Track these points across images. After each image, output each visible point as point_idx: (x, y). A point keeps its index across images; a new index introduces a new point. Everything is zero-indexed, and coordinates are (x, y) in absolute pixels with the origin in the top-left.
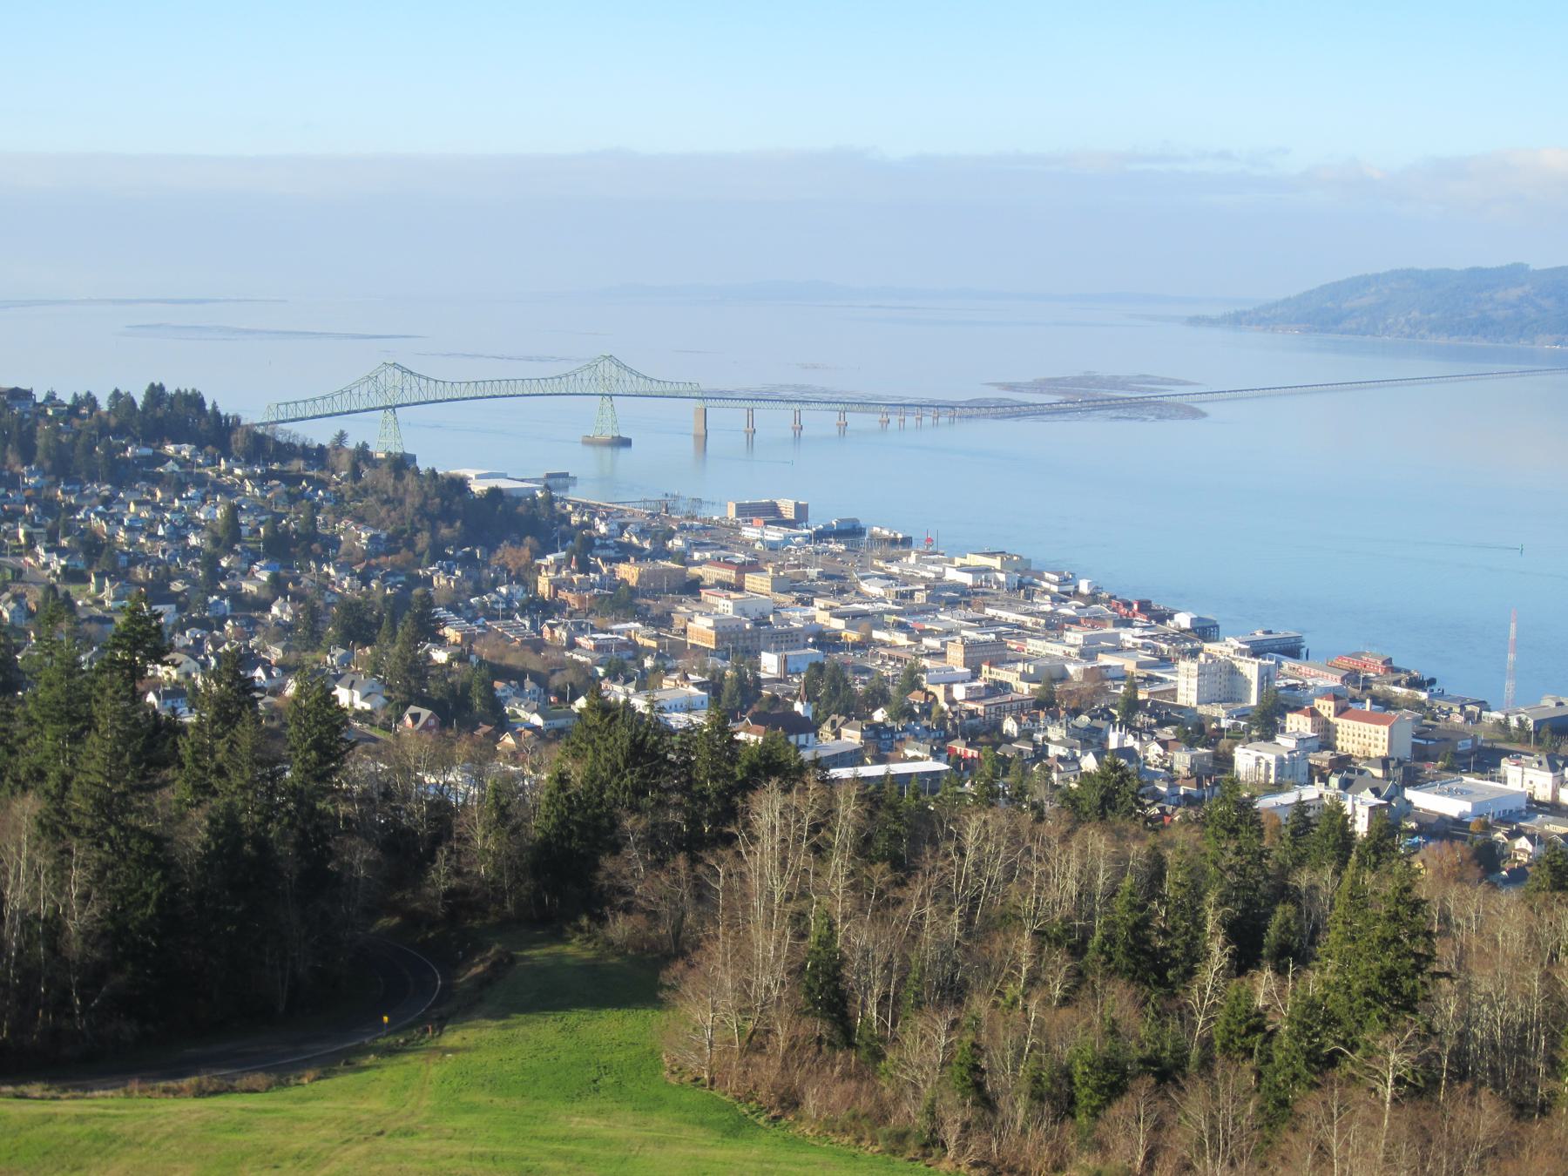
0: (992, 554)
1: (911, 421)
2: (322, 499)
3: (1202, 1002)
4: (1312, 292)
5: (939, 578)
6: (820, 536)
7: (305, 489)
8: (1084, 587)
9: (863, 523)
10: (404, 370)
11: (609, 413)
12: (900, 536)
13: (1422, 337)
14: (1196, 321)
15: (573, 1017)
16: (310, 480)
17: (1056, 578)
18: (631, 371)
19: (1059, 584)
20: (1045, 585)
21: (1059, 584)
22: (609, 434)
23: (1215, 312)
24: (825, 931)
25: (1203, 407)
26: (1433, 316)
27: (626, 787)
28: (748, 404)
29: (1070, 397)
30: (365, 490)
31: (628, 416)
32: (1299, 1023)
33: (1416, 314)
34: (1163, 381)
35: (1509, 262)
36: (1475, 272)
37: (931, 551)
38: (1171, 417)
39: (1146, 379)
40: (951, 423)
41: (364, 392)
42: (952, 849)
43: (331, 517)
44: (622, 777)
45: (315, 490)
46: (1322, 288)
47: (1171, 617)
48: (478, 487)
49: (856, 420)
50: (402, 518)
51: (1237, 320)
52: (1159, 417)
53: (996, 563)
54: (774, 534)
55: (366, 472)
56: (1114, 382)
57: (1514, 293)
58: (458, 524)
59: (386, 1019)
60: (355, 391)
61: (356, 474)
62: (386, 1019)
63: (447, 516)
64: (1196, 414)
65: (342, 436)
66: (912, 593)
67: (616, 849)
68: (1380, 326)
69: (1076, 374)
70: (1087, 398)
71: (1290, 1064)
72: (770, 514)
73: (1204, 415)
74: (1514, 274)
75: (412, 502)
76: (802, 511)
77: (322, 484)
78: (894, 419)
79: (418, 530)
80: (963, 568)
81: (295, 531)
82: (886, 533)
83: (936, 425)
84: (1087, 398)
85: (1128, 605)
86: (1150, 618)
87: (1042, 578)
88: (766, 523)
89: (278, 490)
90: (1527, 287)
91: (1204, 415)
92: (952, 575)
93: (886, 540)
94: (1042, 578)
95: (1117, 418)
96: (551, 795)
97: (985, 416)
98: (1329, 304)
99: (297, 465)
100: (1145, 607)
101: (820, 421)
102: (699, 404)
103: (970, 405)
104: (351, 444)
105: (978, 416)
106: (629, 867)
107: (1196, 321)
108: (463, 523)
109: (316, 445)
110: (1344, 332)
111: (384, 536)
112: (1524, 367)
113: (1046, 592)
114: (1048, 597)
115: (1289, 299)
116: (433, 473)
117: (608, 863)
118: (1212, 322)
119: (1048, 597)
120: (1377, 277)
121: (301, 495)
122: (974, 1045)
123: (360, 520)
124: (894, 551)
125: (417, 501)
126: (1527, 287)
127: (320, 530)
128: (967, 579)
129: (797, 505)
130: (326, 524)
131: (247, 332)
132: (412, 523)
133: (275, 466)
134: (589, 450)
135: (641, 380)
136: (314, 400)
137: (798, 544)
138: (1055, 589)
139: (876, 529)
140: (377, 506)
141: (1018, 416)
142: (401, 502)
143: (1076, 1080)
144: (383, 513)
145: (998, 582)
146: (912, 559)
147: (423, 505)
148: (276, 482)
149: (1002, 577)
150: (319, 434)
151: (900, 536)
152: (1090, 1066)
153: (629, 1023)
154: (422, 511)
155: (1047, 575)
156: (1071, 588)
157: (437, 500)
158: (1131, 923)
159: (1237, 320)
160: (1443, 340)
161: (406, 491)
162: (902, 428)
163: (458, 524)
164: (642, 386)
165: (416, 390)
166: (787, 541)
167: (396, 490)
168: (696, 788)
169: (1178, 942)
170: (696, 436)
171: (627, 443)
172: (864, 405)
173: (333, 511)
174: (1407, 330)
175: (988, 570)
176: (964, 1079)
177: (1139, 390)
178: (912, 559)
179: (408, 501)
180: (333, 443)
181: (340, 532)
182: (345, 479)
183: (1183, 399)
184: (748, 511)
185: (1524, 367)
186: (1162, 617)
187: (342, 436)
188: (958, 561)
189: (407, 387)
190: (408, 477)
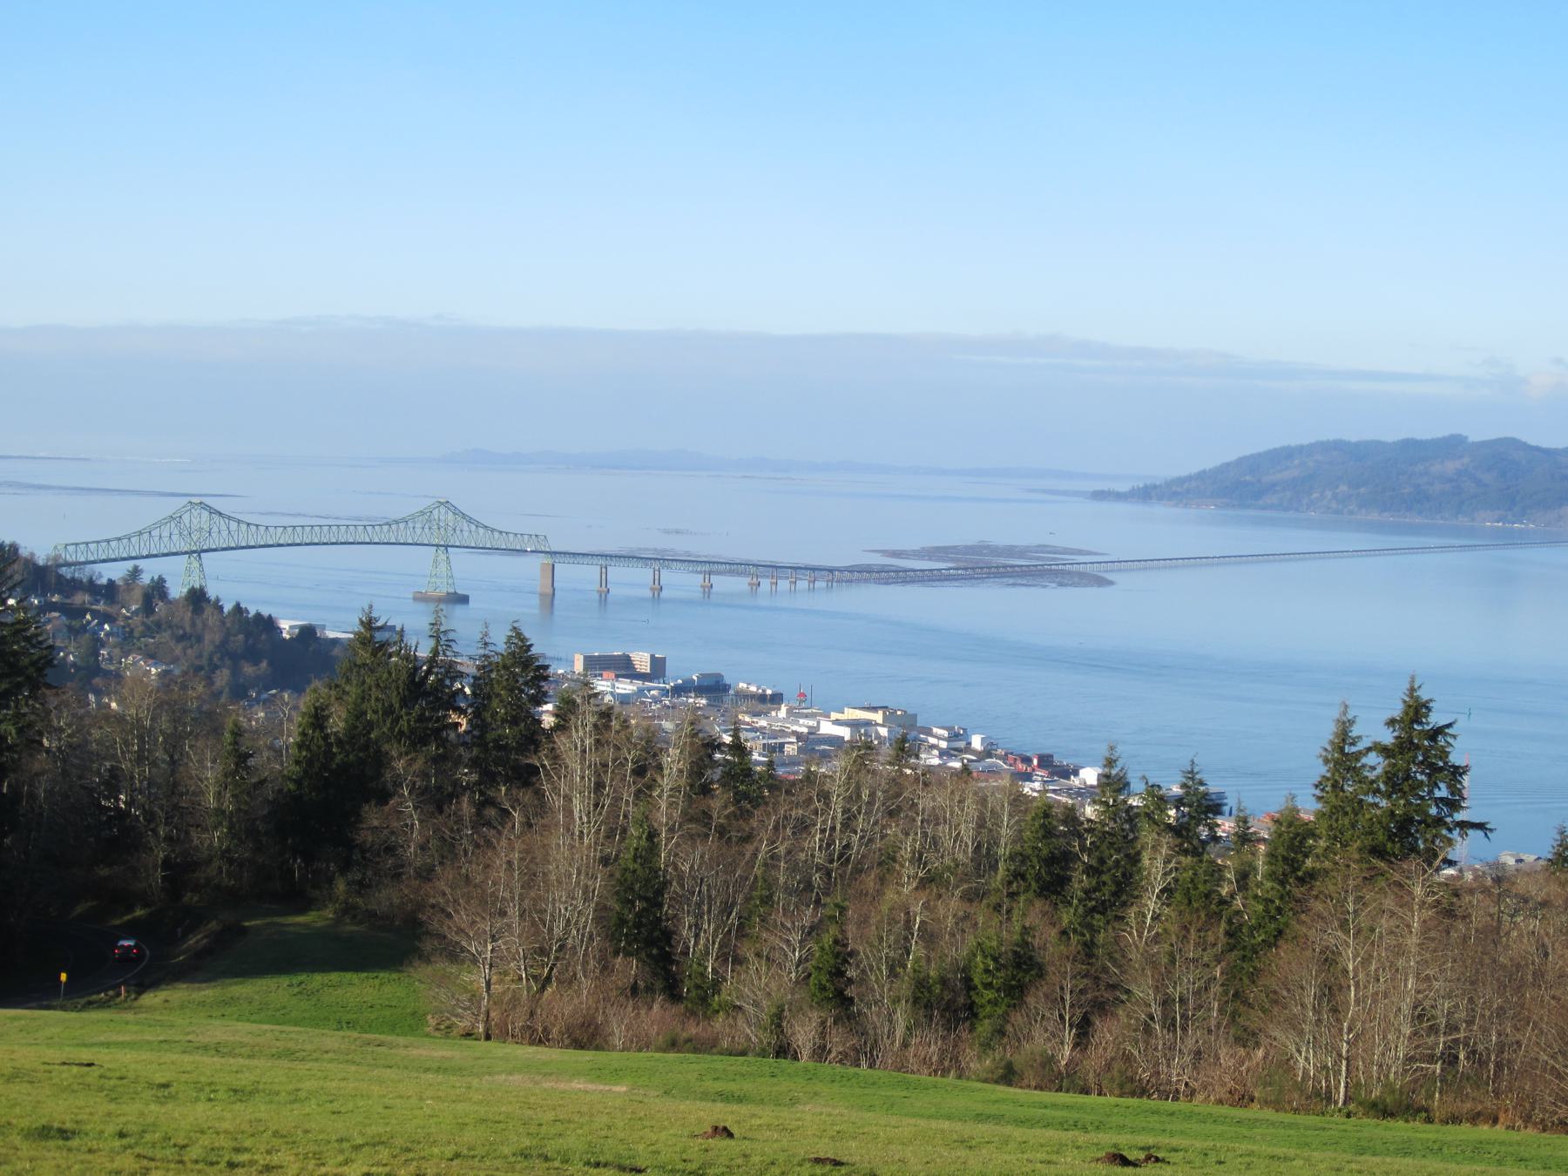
0: (874, 709)
1: (784, 585)
2: (108, 634)
3: (1140, 937)
4: (1228, 464)
5: (813, 731)
6: (678, 691)
7: (89, 622)
8: (977, 742)
9: (727, 681)
10: (213, 511)
11: (443, 567)
12: (769, 692)
13: (1351, 513)
14: (1100, 495)
15: (318, 979)
16: (95, 614)
17: (945, 733)
18: (470, 521)
19: (949, 740)
20: (932, 741)
21: (949, 740)
22: (443, 590)
23: (1123, 487)
24: (643, 843)
25: (1110, 577)
26: (1362, 490)
27: (401, 733)
28: (602, 562)
29: (962, 565)
30: (158, 625)
31: (467, 570)
32: (1285, 859)
33: (1343, 488)
34: (1066, 551)
35: (1446, 433)
36: (1408, 445)
37: (803, 703)
38: (1074, 585)
39: (1042, 548)
40: (829, 588)
41: (166, 534)
42: (814, 794)
43: (117, 651)
44: (397, 720)
45: (101, 624)
46: (1240, 461)
47: (1076, 773)
48: (287, 626)
49: (722, 583)
50: (200, 656)
51: (1147, 494)
52: (1061, 585)
53: (878, 717)
54: (626, 687)
55: (160, 607)
56: (1010, 551)
57: (1451, 466)
58: (264, 664)
59: (64, 977)
60: (155, 533)
61: (148, 607)
62: (64, 977)
63: (253, 655)
64: (1101, 582)
65: (136, 572)
66: (782, 745)
67: (383, 797)
68: (1305, 501)
69: (969, 543)
70: (978, 566)
71: (1273, 918)
72: (623, 667)
73: (1111, 583)
74: (1452, 445)
75: (211, 638)
76: (658, 666)
77: (108, 618)
78: (765, 584)
79: (217, 667)
80: (837, 722)
81: (74, 664)
82: (753, 689)
83: (812, 590)
84: (978, 566)
85: (1027, 760)
86: (1052, 774)
87: (929, 733)
88: (617, 676)
89: (57, 623)
90: (1466, 460)
91: (1111, 583)
92: (827, 728)
93: (753, 696)
94: (929, 733)
95: (1014, 585)
96: (304, 734)
97: (866, 581)
98: (1248, 478)
99: (81, 598)
100: (1046, 761)
101: (682, 583)
102: (548, 560)
103: (851, 569)
104: (146, 579)
105: (858, 581)
106: (405, 821)
107: (1100, 495)
108: (270, 664)
109: (104, 581)
110: (1263, 508)
111: (177, 672)
112: (1457, 542)
113: (933, 747)
114: (936, 752)
115: (1204, 472)
116: (238, 609)
117: (373, 817)
118: (1118, 496)
119: (936, 752)
120: (1301, 449)
121: (84, 628)
122: (836, 942)
123: (151, 656)
124: (761, 707)
125: (218, 638)
126: (1466, 460)
127: (103, 666)
128: (845, 733)
129: (652, 657)
130: (111, 659)
131: (40, 487)
132: (210, 659)
133: (56, 598)
134: (421, 607)
135: (481, 531)
136: (108, 541)
137: (653, 697)
138: (943, 745)
139: (742, 685)
140: (172, 644)
141: (905, 582)
142: (200, 639)
143: (977, 981)
144: (178, 650)
145: (878, 737)
146: (783, 713)
147: (224, 642)
148: (56, 614)
149: (883, 732)
150: (114, 572)
151: (769, 692)
152: (995, 959)
153: (387, 989)
154: (222, 647)
155: (935, 730)
156: (962, 744)
157: (241, 637)
158: (1045, 852)
159: (1147, 494)
160: (1374, 516)
161: (205, 625)
162: (773, 593)
163: (264, 664)
164: (482, 538)
165: (466, 534)
166: (641, 691)
167: (193, 625)
168: (490, 736)
169: (1105, 878)
170: (542, 595)
171: (464, 600)
172: (735, 567)
173: (120, 645)
174: (1334, 505)
175: (868, 723)
176: (823, 988)
177: (1038, 559)
178: (783, 713)
179: (207, 638)
180: (126, 580)
181: (126, 668)
182: (136, 613)
183: (1081, 568)
184: (597, 664)
185: (1457, 542)
186: (1067, 772)
187: (136, 572)
188: (834, 716)
189: (215, 529)
190: (208, 610)
